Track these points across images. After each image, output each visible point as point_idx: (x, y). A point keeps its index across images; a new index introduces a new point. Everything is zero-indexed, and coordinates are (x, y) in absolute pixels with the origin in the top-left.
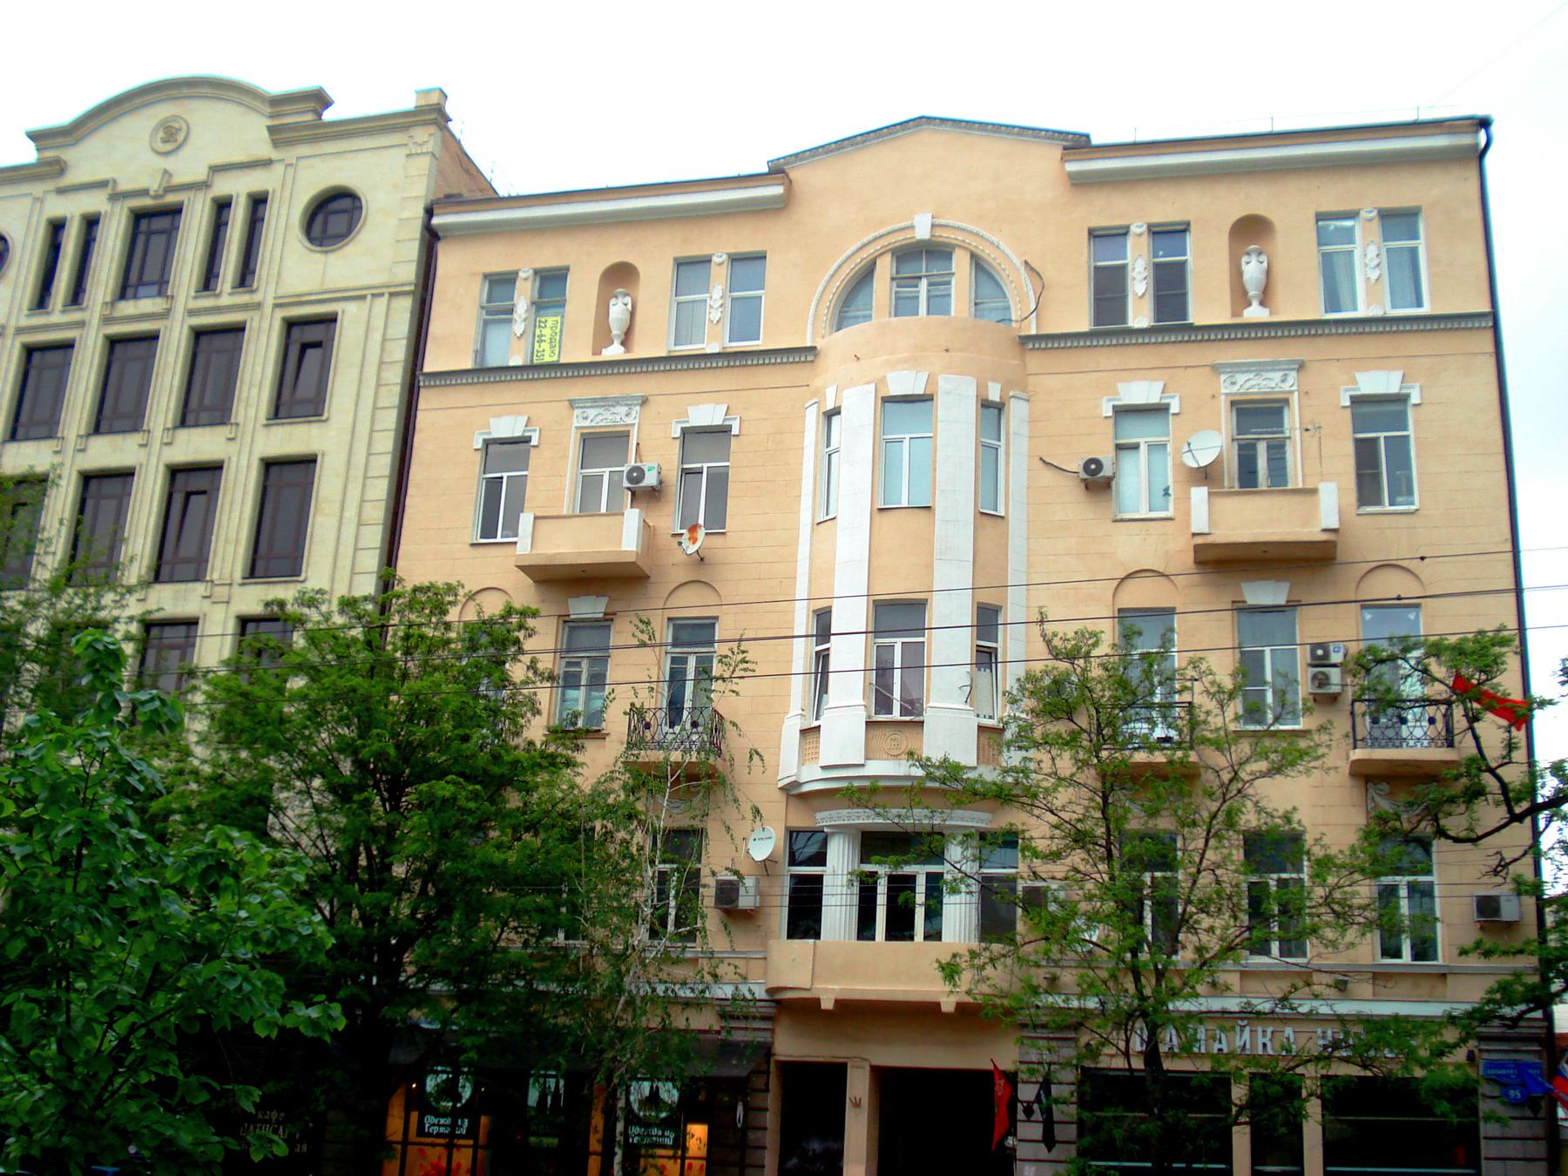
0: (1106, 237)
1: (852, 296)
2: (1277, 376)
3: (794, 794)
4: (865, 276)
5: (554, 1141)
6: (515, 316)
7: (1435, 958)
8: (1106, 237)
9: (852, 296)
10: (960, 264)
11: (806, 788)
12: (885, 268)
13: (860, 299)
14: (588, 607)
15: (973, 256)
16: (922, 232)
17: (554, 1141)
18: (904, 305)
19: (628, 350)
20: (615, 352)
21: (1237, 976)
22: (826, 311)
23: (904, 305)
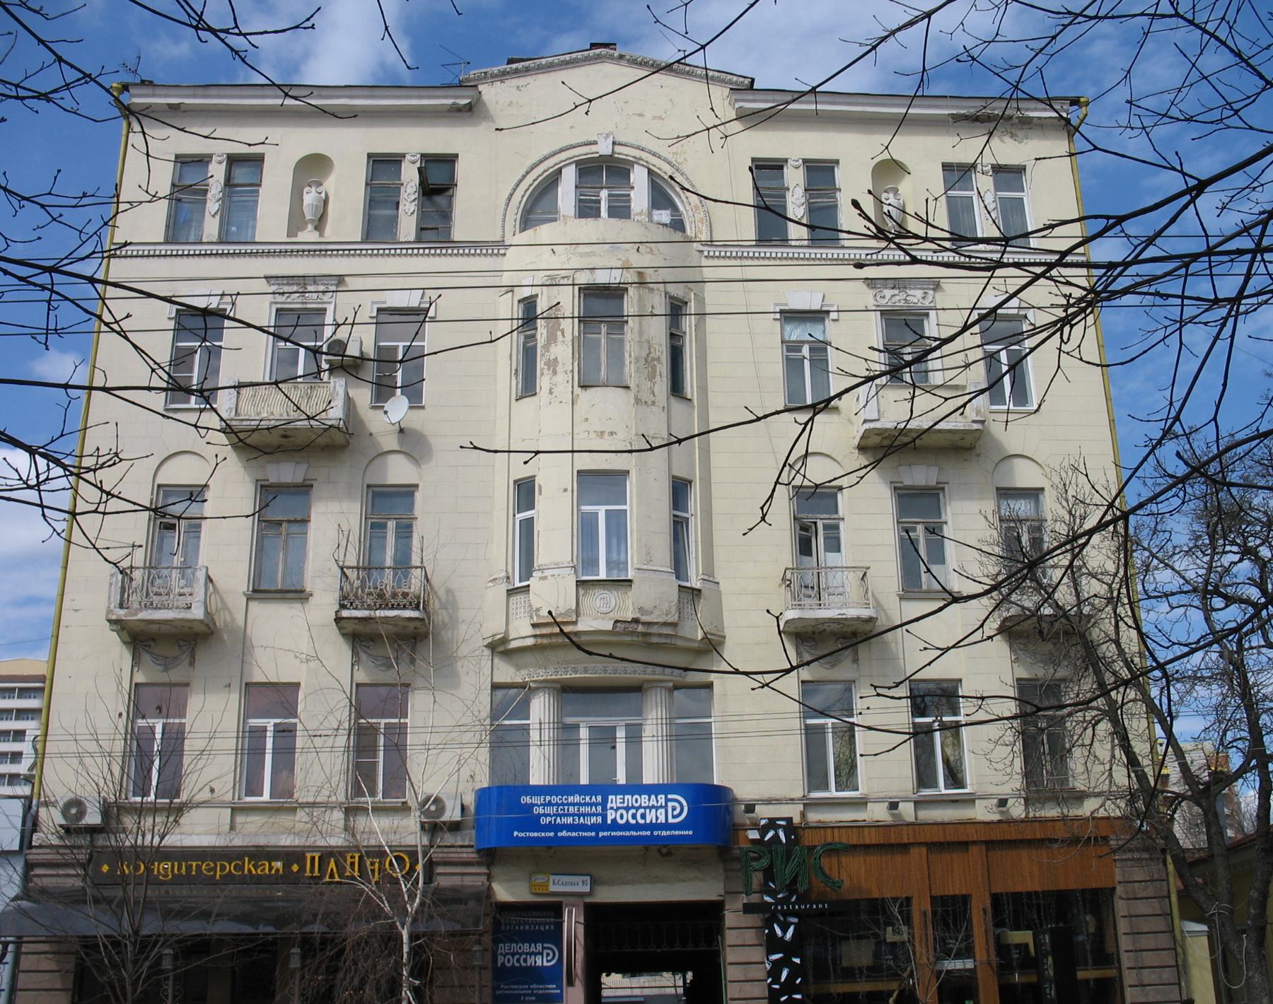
0: (766, 169)
1: (537, 205)
2: (919, 293)
3: (499, 648)
4: (554, 179)
5: (691, 833)
6: (209, 195)
7: (261, 795)
8: (766, 169)
9: (537, 205)
10: (639, 177)
11: (514, 645)
12: (570, 175)
13: (546, 201)
14: (286, 472)
15: (650, 172)
16: (604, 148)
17: (691, 833)
18: (587, 209)
19: (321, 235)
20: (308, 235)
21: (912, 804)
22: (514, 214)
23: (587, 209)
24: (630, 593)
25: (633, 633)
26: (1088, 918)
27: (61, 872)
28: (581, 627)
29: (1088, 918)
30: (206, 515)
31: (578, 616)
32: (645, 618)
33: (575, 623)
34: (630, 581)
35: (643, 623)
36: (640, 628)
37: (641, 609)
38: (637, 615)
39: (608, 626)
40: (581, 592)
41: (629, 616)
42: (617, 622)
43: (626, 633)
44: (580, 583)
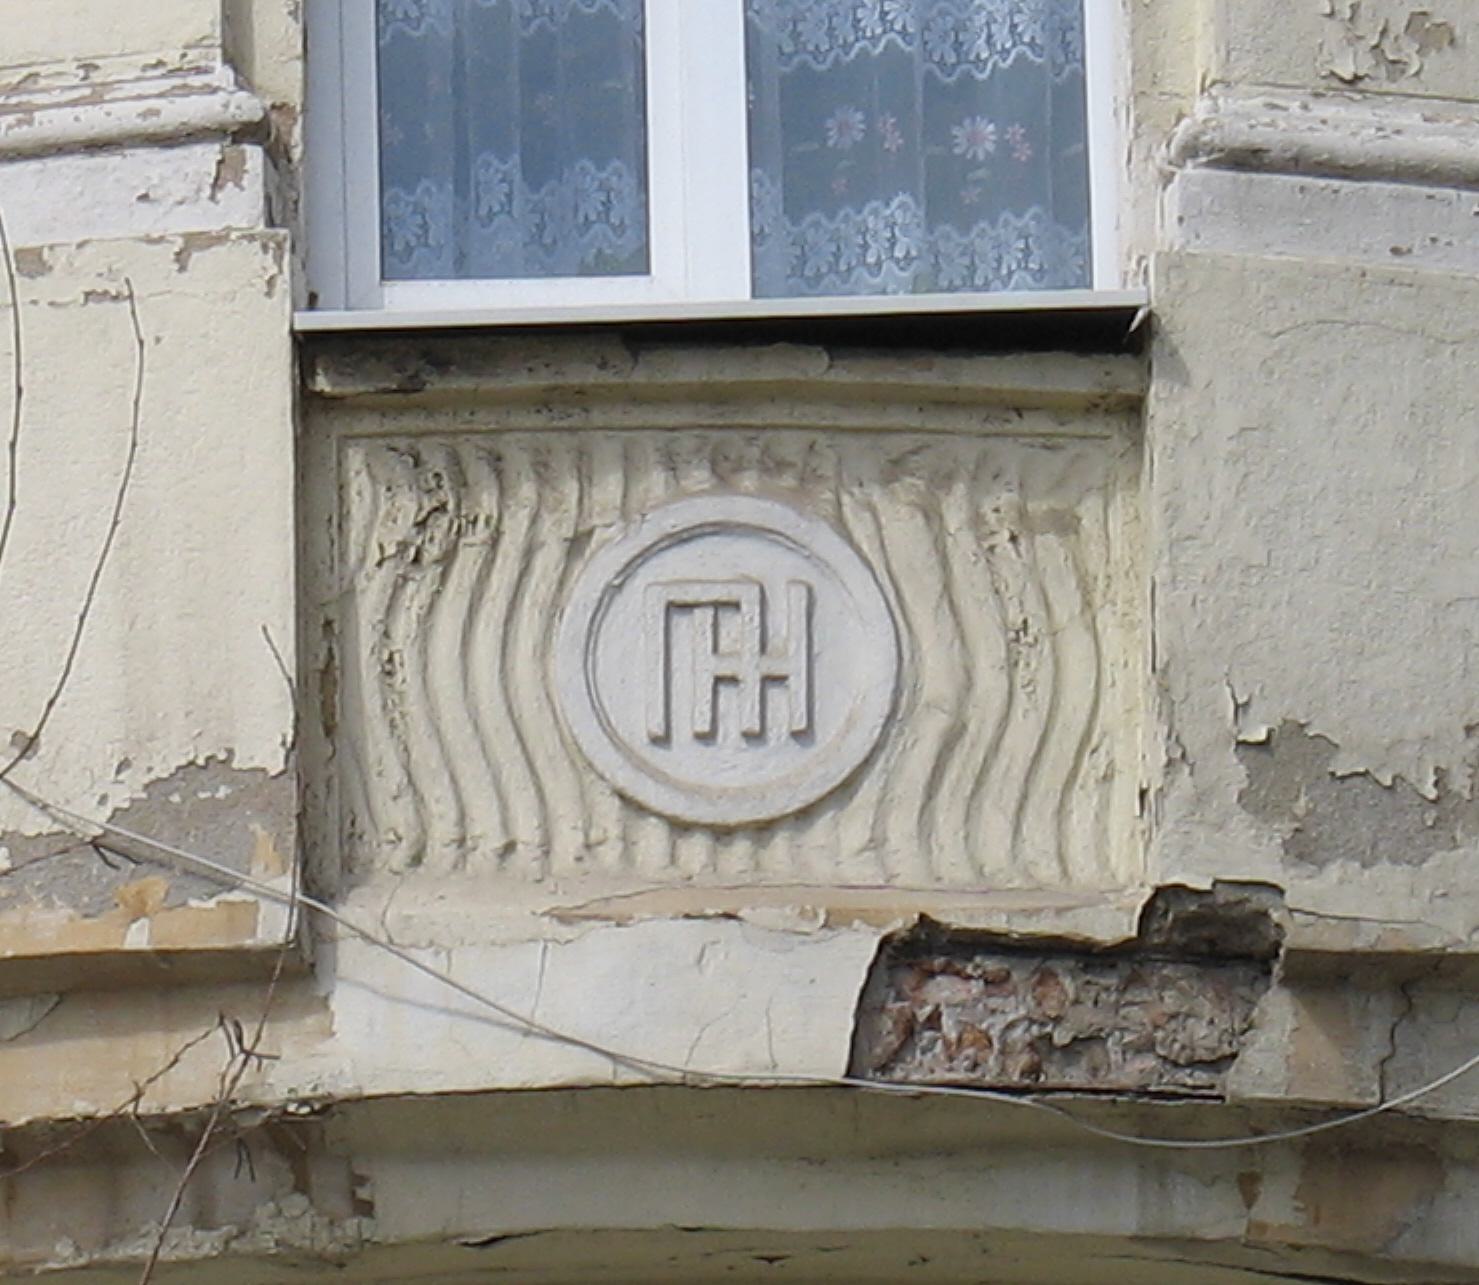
24: (1125, 528)
25: (1167, 1126)
26: (256, 827)
27: (848, 420)
28: (370, 1037)
29: (256, 827)
30: (31, 733)
31: (326, 860)
32: (1346, 901)
33: (287, 976)
34: (1115, 334)
35: (1332, 978)
36: (1280, 1052)
37: (1279, 757)
38: (1231, 853)
39: (793, 1018)
40: (379, 510)
41: (1105, 866)
42: (916, 951)
43: (1039, 1119)
44: (347, 376)
